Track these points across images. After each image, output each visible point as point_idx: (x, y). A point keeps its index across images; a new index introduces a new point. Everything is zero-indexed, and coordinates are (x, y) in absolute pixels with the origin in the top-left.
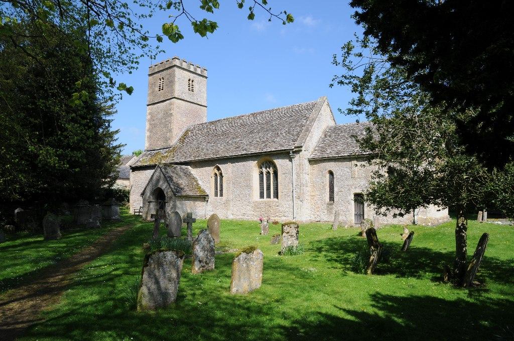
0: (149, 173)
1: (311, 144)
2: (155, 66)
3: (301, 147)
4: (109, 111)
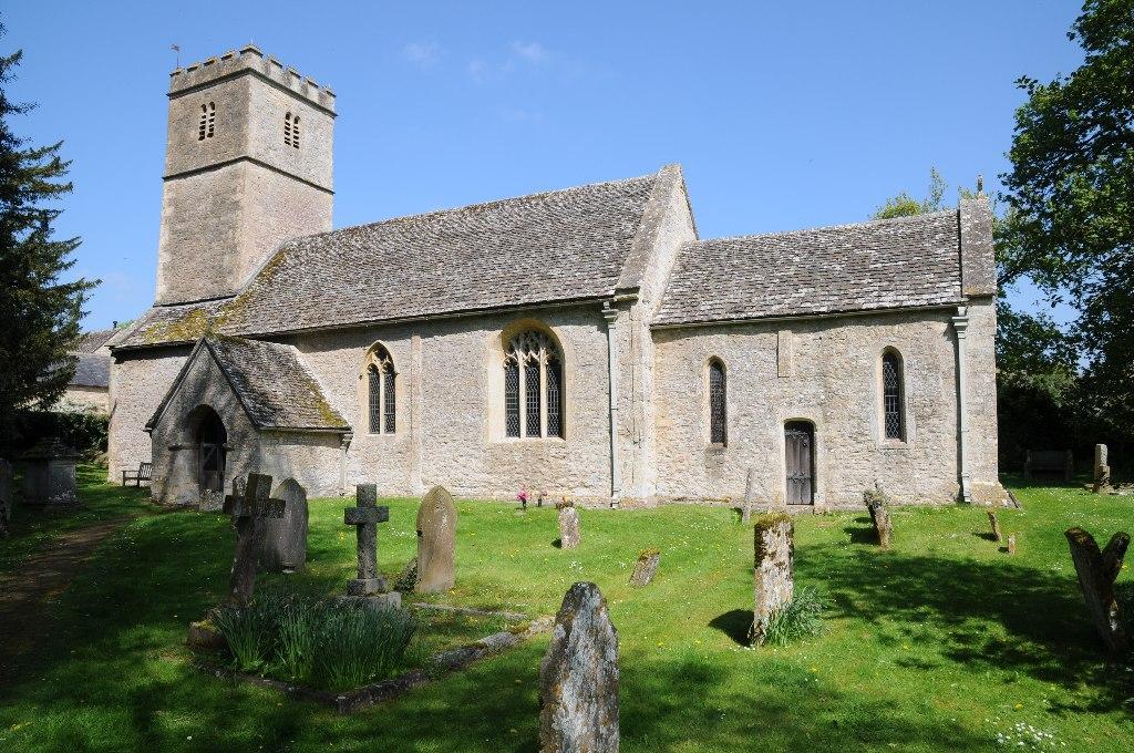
0: (171, 366)
1: (656, 281)
2: (190, 70)
3: (636, 289)
4: (46, 180)
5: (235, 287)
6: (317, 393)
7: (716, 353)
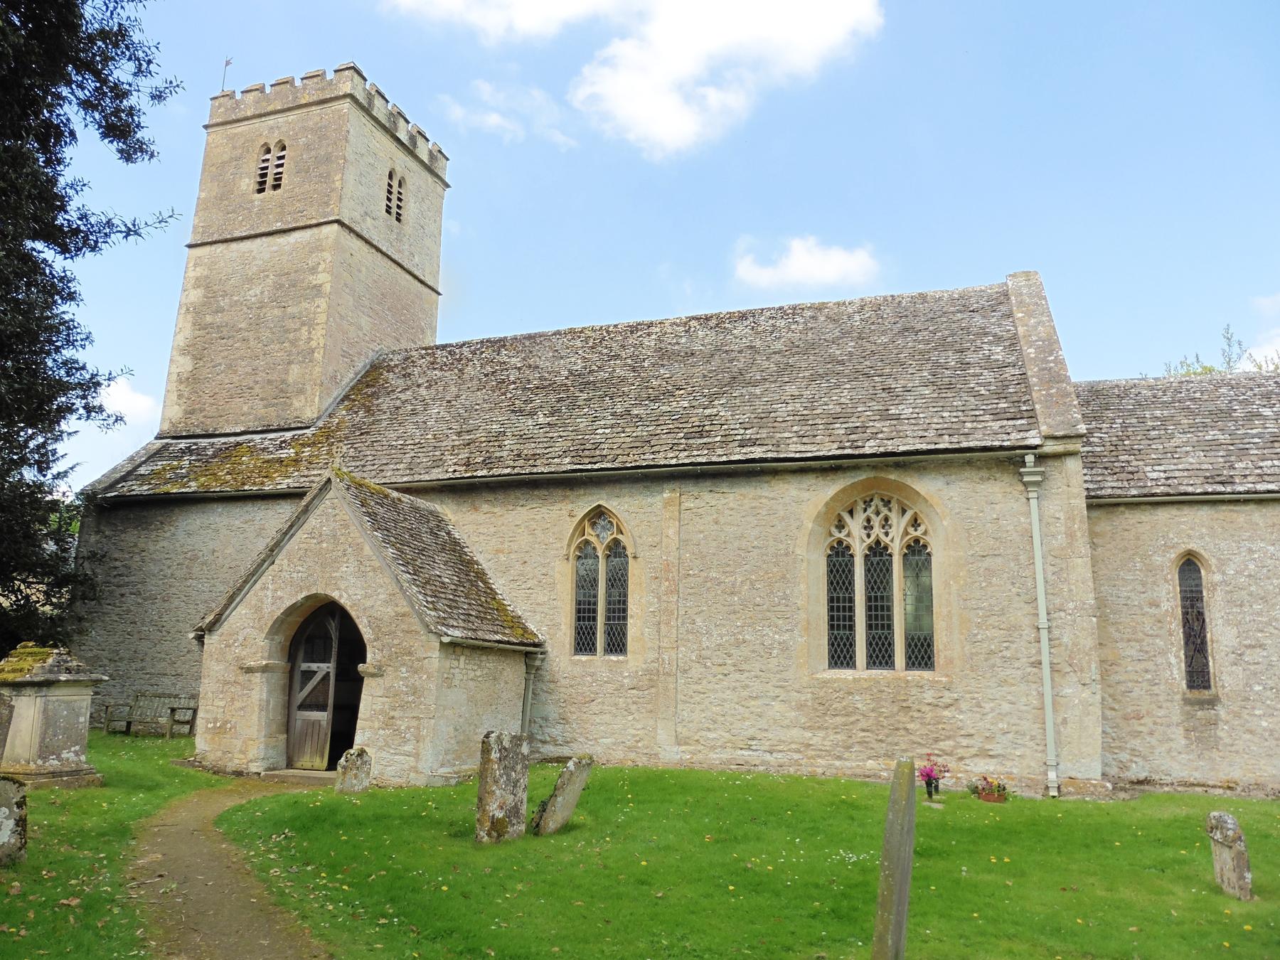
6: (485, 583)
7: (1192, 546)
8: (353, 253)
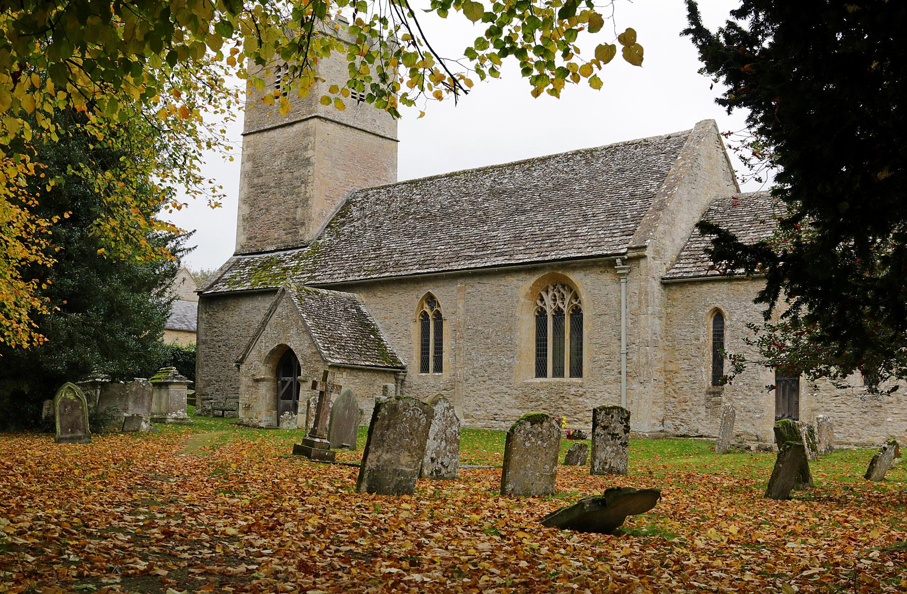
5: (307, 238)
7: (718, 305)
8: (329, 133)
